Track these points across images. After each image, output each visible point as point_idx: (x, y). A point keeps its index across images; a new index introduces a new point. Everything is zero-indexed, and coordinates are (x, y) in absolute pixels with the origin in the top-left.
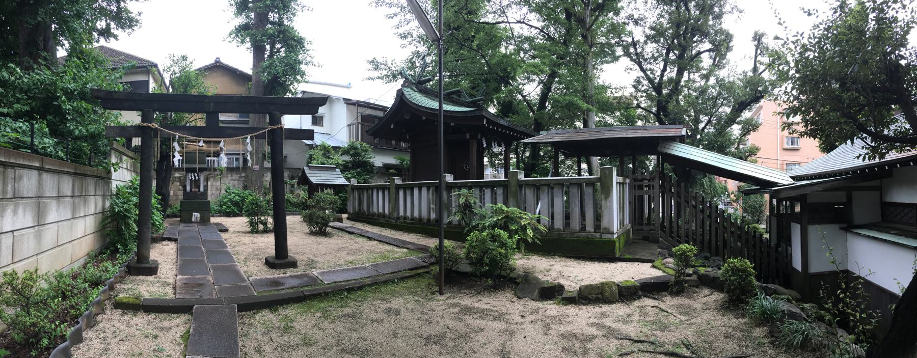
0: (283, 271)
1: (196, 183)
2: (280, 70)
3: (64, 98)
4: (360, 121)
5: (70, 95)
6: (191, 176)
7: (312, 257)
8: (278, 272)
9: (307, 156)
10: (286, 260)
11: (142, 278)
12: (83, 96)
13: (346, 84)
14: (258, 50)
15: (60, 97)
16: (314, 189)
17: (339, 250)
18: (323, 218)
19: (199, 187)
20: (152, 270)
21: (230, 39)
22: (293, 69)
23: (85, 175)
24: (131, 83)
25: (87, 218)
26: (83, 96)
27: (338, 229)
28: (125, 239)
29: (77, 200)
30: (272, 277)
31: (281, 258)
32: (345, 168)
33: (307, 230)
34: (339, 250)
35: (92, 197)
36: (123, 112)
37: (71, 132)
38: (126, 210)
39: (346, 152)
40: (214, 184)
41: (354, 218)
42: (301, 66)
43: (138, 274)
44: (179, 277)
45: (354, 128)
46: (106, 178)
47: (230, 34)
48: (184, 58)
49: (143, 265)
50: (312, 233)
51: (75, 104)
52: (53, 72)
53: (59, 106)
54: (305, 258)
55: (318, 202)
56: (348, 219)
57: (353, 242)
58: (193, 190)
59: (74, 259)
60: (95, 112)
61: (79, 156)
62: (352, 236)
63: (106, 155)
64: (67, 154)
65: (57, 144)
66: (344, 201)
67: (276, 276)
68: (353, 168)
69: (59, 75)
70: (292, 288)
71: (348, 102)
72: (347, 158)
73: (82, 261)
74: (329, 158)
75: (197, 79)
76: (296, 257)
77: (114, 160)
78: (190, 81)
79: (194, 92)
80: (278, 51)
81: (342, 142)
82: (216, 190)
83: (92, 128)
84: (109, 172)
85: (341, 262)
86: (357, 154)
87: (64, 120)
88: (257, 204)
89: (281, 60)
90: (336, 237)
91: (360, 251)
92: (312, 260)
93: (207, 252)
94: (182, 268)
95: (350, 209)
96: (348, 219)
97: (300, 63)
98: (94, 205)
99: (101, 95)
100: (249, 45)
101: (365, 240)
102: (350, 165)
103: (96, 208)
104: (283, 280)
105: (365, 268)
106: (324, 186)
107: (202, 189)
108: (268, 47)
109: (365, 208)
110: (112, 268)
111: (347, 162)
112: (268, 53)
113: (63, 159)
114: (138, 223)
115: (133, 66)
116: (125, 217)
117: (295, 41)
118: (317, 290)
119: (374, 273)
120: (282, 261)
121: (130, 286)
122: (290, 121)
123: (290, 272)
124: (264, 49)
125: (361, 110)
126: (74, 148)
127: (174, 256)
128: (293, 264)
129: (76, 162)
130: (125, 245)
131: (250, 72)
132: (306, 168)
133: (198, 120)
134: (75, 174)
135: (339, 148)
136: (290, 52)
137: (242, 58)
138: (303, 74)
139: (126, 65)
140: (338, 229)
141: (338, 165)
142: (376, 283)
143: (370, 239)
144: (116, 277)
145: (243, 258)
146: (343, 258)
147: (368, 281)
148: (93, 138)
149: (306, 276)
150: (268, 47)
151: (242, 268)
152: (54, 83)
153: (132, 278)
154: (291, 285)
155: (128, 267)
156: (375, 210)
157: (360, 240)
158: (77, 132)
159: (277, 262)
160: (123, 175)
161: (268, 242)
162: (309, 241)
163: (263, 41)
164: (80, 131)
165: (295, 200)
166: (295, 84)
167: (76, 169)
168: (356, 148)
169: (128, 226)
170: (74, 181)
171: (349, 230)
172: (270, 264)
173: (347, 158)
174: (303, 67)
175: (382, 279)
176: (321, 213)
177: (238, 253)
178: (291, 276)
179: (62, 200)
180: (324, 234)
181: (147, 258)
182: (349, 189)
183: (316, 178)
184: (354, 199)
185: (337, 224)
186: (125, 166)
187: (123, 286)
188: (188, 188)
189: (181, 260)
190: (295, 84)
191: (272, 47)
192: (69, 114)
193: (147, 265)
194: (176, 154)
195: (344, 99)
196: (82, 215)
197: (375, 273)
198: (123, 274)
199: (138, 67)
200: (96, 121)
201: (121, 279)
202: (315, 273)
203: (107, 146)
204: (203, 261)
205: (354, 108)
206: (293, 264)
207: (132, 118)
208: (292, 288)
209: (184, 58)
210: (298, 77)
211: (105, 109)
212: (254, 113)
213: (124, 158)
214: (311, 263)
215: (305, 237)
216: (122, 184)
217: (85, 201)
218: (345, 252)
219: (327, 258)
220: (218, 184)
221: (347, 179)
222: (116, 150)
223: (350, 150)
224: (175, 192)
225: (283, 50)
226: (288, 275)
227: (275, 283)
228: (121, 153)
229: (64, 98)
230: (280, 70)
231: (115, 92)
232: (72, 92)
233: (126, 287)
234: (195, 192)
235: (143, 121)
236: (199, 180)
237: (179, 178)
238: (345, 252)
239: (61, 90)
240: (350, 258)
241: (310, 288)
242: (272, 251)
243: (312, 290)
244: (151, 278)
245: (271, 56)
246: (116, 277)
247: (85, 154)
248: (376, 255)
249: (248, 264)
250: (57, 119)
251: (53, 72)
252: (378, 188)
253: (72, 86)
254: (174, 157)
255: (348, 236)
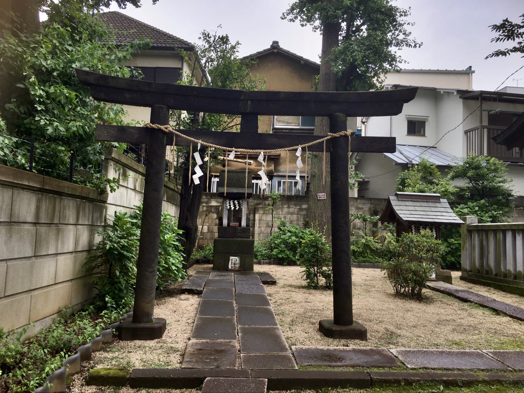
0: (343, 341)
1: (236, 215)
2: (359, 56)
3: (33, 79)
4: (485, 123)
5: (45, 76)
6: (230, 205)
7: (392, 328)
8: (336, 342)
9: (398, 179)
10: (349, 327)
11: (138, 342)
12: (66, 79)
13: (464, 68)
14: (330, 32)
15: (28, 77)
16: (403, 227)
17: (439, 322)
18: (415, 273)
19: (240, 220)
20: (156, 331)
21: (291, 16)
22: (378, 54)
23: (60, 194)
24: (142, 68)
25: (61, 258)
26: (66, 79)
27: (443, 292)
28: (120, 290)
29: (43, 229)
30: (326, 348)
31: (342, 323)
32: (457, 200)
33: (391, 290)
34: (439, 322)
35: (71, 227)
36: (126, 107)
37: (42, 130)
38: (123, 247)
39: (460, 174)
40: (264, 217)
41: (477, 277)
42: (390, 49)
43: (133, 338)
44: (193, 341)
45: (475, 136)
46: (99, 200)
47: (292, 9)
48: (224, 40)
49: (142, 325)
50: (398, 295)
51: (52, 90)
52: (21, 41)
53: (26, 91)
54: (381, 328)
55: (408, 248)
56: (462, 278)
57: (464, 314)
58: (232, 224)
59: (34, 317)
60: (84, 105)
61: (53, 166)
62: (466, 306)
63: (101, 167)
64: (31, 160)
65: (17, 146)
66: (455, 251)
67: (332, 348)
68: (472, 198)
69: (28, 47)
70: (353, 366)
71: (467, 96)
72: (463, 183)
73: (48, 321)
74: (432, 183)
75: (240, 69)
76: (368, 326)
77: (112, 174)
78: (230, 73)
79: (236, 87)
80: (358, 29)
81: (454, 158)
82: (265, 227)
83: (75, 125)
84: (103, 192)
85: (441, 341)
86: (479, 177)
87: (32, 112)
88: (316, 246)
89: (362, 42)
90: (438, 304)
91: (475, 328)
92: (392, 333)
93: (240, 310)
94: (199, 331)
95: (466, 263)
96: (462, 278)
97: (389, 44)
98: (75, 237)
99: (91, 79)
100: (317, 23)
101: (487, 312)
102: (468, 194)
103: (76, 243)
104: (343, 354)
105: (480, 356)
106: (419, 225)
107: (244, 223)
108: (344, 25)
109: (492, 263)
110: (89, 329)
111: (462, 190)
112: (343, 33)
113: (25, 169)
114: (139, 265)
115: (146, 46)
116: (121, 258)
117: (382, 13)
118: (394, 374)
119: (496, 365)
120: (344, 328)
121: (117, 354)
122: (375, 127)
123: (354, 345)
124: (339, 28)
125: (486, 106)
126: (43, 154)
127: (193, 314)
128: (361, 334)
129: (48, 174)
130: (117, 298)
131: (318, 61)
132: (392, 198)
133: (233, 124)
134: (41, 191)
135: (449, 167)
136: (375, 29)
137: (307, 42)
138: (392, 59)
139: (136, 42)
140: (443, 292)
141: (445, 194)
142: (500, 382)
143: (497, 312)
144: (95, 343)
145: (289, 319)
146: (444, 336)
147: (482, 376)
148: (78, 141)
149: (379, 353)
150: (344, 25)
151: (284, 333)
152: (19, 57)
153: (122, 343)
154: (352, 363)
155: (118, 329)
156: (510, 267)
157: (479, 312)
158: (50, 130)
159: (336, 328)
160: (125, 197)
161: (324, 302)
162: (392, 306)
163: (337, 17)
164: (56, 129)
165: (379, 246)
166: (382, 76)
167: (44, 182)
168: (478, 167)
169: (125, 271)
170: (39, 201)
171: (460, 295)
172: (325, 330)
173: (463, 183)
174: (393, 49)
175: (512, 377)
176: (413, 266)
177: (283, 314)
178: (354, 350)
179: (16, 227)
180: (418, 297)
181: (149, 314)
182: (463, 231)
183: (406, 212)
184: (473, 248)
185: (442, 285)
186: (131, 185)
187: (105, 354)
188: (225, 222)
189: (200, 319)
190: (382, 76)
191: (349, 26)
192: (40, 103)
193: (148, 325)
194: (197, 169)
195: (459, 92)
196: (52, 251)
197: (499, 366)
198: (109, 338)
199: (154, 48)
200: (82, 117)
201: (105, 345)
202: (394, 351)
203: (100, 153)
204: (232, 319)
205: (475, 104)
206: (361, 334)
207: (138, 116)
208: (353, 366)
209: (224, 40)
210: (386, 65)
211: (99, 100)
212: (318, 116)
213: (131, 174)
214: (390, 337)
215: (390, 300)
216: (123, 210)
217: (58, 231)
218: (449, 328)
219: (417, 332)
220: (269, 218)
221: (462, 215)
222: (117, 162)
223: (470, 170)
224: (205, 226)
225: (364, 28)
226: (351, 347)
227: (329, 357)
228: (125, 166)
229: (33, 79)
230: (359, 56)
231: (117, 78)
232: (49, 72)
233: (110, 355)
234: (234, 227)
235: (152, 122)
236: (240, 210)
237: (216, 207)
238: (449, 328)
239: (31, 67)
240: (457, 337)
241: (382, 370)
242: (329, 314)
243: (385, 374)
244: (152, 343)
245: (347, 37)
246: (95, 343)
247: (63, 162)
248: (505, 339)
249: (293, 328)
250: (22, 109)
251: (21, 41)
252: (515, 230)
253: (49, 63)
254: (194, 173)
255: (457, 304)
